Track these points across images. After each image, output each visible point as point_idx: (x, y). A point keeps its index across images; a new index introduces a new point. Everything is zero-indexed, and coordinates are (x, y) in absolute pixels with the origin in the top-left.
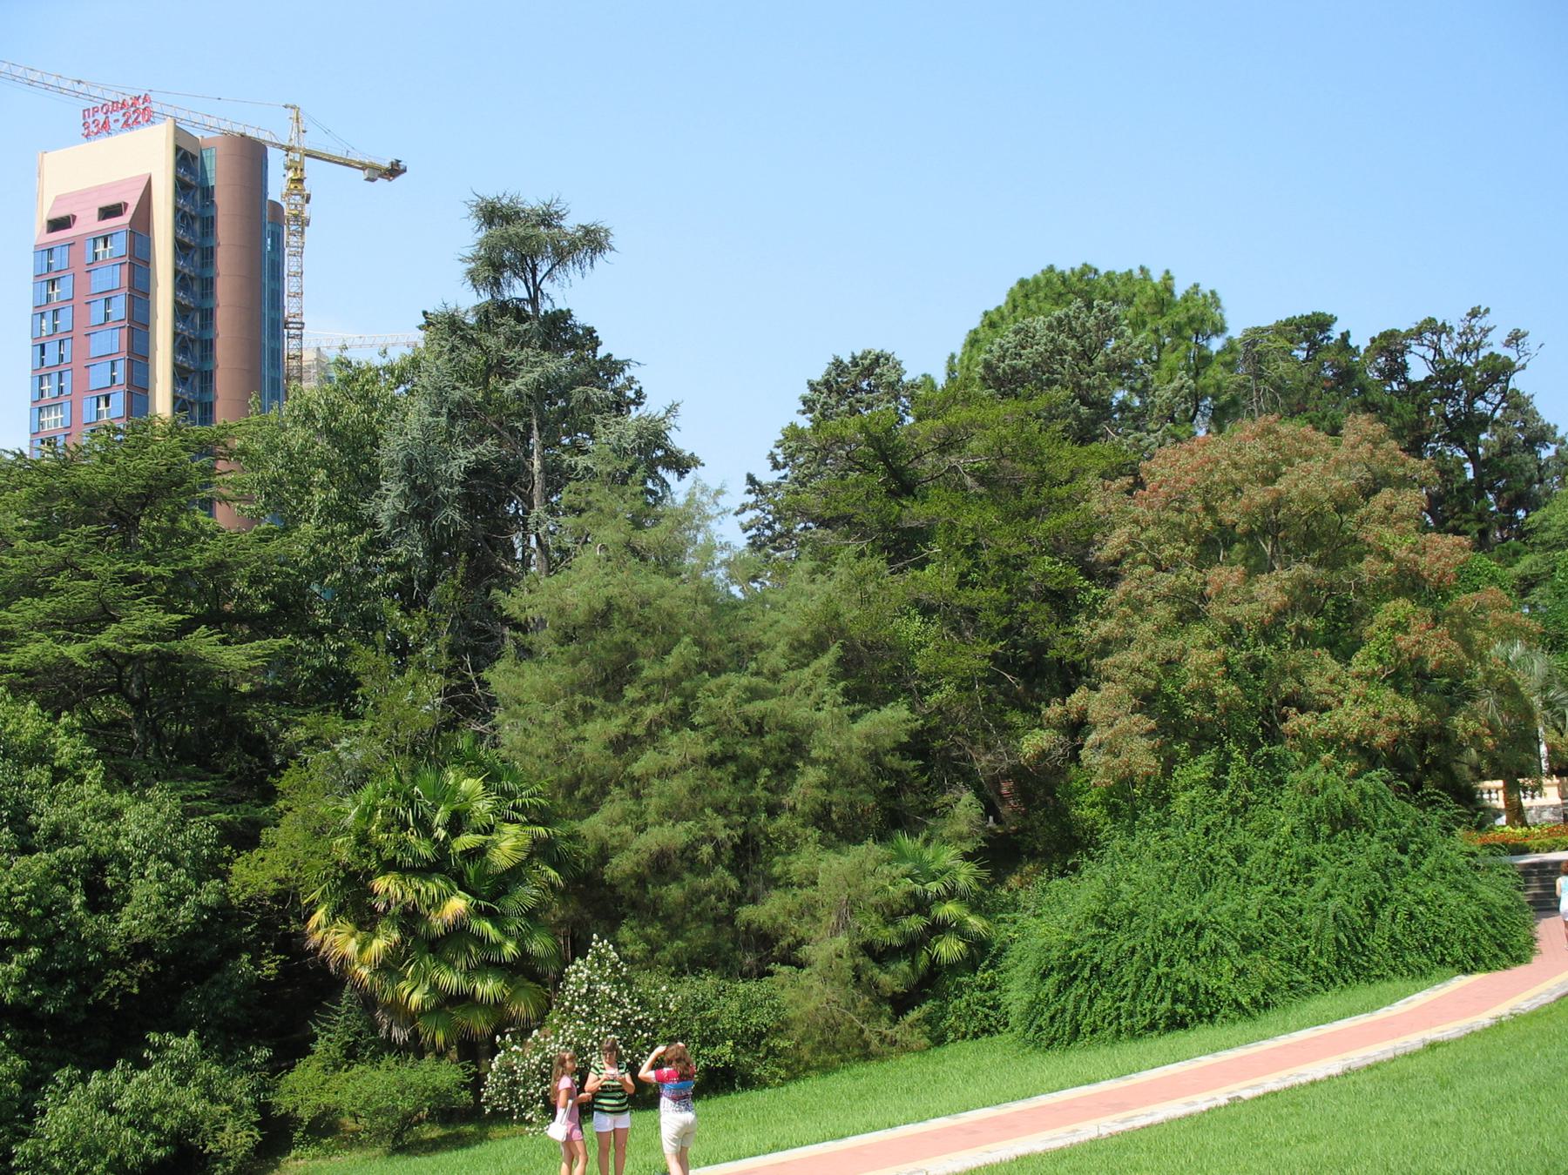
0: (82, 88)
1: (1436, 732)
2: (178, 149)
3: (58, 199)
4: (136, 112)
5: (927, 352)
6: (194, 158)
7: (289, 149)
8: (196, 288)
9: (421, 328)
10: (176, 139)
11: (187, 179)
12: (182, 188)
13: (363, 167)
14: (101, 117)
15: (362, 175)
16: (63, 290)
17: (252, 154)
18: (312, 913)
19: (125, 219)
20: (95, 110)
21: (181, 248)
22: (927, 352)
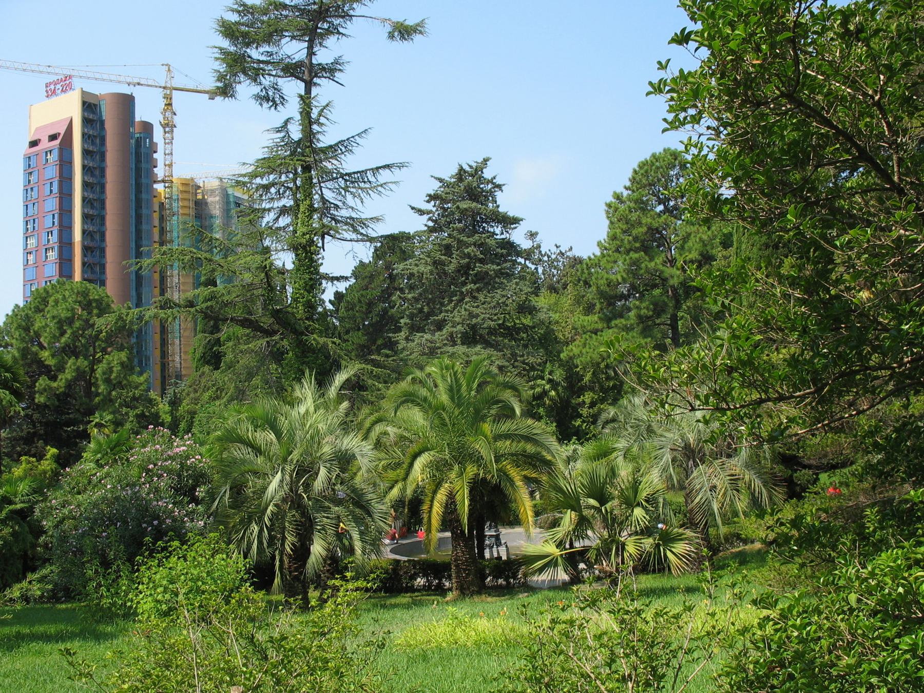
0: (49, 70)
2: (84, 103)
3: (37, 129)
4: (65, 84)
7: (164, 88)
8: (97, 173)
9: (681, 71)
10: (82, 97)
12: (86, 121)
14: (52, 87)
15: (207, 96)
16: (33, 178)
17: (126, 103)
18: (267, 509)
19: (57, 142)
20: (50, 83)
21: (86, 153)
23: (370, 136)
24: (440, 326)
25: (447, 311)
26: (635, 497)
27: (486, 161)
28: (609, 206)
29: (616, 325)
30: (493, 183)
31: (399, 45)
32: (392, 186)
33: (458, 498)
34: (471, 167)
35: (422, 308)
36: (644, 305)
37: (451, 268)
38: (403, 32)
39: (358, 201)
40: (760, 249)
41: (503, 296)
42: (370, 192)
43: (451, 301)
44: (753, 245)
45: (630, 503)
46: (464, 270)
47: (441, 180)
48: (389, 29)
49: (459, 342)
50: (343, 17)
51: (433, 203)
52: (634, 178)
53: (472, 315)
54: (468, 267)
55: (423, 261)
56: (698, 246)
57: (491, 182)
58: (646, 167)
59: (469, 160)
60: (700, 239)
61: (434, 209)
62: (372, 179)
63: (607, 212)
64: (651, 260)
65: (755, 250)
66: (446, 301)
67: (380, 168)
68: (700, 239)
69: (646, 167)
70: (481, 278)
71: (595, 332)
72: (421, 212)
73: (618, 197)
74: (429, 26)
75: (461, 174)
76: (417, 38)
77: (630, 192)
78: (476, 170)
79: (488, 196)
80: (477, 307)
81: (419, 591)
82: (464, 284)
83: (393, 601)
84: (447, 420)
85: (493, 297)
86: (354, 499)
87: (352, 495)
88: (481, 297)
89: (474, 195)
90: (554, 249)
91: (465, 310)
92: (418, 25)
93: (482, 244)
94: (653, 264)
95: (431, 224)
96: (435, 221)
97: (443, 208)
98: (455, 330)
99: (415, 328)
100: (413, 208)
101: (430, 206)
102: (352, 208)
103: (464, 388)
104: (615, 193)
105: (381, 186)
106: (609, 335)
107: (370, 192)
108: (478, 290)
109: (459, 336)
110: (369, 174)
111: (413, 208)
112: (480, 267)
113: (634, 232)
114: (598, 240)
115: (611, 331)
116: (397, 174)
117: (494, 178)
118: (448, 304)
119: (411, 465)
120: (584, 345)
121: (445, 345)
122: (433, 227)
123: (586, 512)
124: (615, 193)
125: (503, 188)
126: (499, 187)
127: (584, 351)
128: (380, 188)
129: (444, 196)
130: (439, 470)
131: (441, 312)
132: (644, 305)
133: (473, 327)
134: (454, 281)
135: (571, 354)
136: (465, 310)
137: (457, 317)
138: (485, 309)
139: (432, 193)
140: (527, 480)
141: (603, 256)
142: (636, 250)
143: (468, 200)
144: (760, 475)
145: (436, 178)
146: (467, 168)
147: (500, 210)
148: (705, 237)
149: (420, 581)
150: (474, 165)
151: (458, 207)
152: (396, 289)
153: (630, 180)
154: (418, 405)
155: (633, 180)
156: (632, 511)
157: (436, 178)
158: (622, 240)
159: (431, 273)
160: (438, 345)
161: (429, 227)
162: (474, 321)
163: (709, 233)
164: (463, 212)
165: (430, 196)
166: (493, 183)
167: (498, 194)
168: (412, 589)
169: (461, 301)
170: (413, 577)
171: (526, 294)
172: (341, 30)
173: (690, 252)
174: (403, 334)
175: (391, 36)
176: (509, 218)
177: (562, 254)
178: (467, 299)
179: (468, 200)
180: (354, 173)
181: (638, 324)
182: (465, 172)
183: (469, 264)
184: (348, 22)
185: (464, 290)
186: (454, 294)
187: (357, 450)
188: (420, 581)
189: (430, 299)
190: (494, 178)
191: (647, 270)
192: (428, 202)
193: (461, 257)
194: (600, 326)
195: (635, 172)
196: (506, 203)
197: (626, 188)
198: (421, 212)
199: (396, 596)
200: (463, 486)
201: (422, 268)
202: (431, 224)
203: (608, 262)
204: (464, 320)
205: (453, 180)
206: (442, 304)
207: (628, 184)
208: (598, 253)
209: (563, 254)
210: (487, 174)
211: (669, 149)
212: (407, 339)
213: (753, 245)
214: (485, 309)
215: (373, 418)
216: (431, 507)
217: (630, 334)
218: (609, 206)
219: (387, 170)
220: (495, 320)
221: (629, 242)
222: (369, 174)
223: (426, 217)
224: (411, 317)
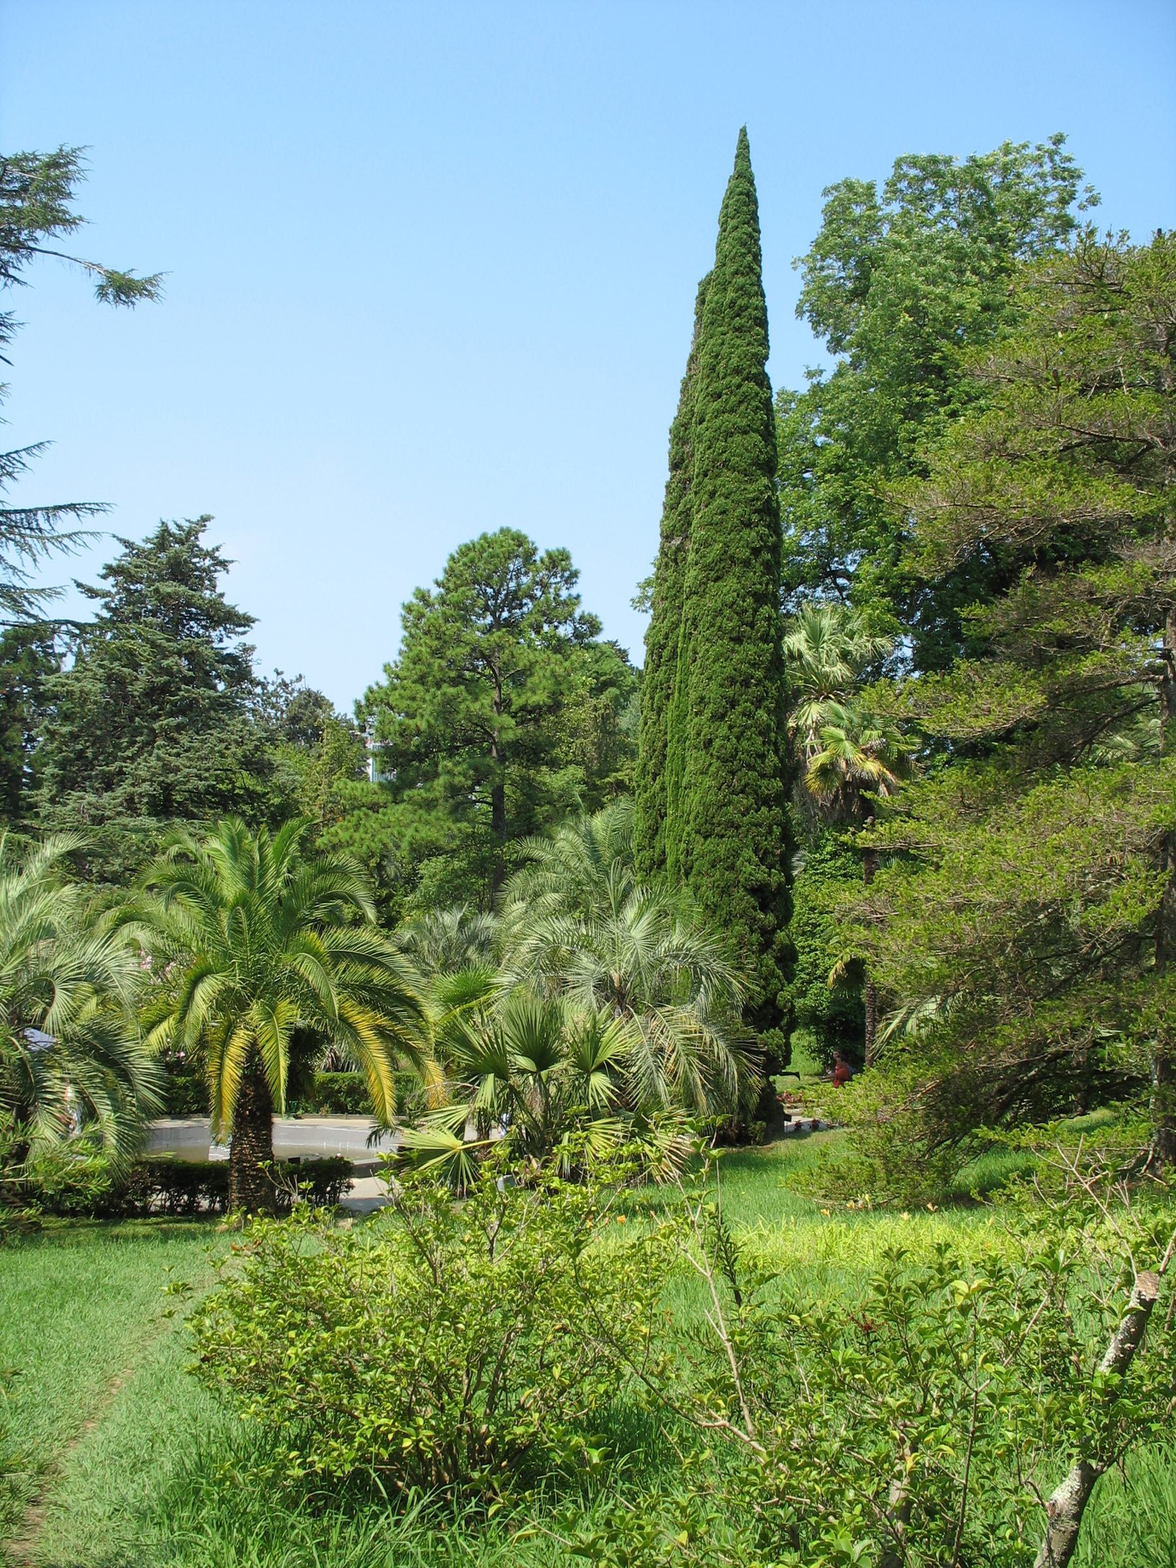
23: (49, 452)
24: (109, 784)
25: (124, 759)
26: (595, 1056)
27: (205, 519)
28: (409, 609)
29: (410, 798)
30: (213, 558)
31: (115, 312)
32: (87, 538)
33: (266, 1054)
34: (180, 527)
35: (82, 751)
36: (459, 769)
37: (137, 689)
38: (121, 288)
39: (27, 557)
40: (721, 686)
41: (221, 741)
42: (48, 545)
43: (132, 743)
44: (710, 679)
45: (585, 1068)
46: (154, 693)
47: (127, 544)
48: (99, 280)
49: (144, 810)
50: (15, 250)
51: (111, 580)
52: (452, 569)
53: (167, 769)
54: (164, 689)
55: (89, 674)
56: (549, 684)
57: (209, 554)
58: (472, 554)
59: (179, 515)
60: (553, 672)
61: (114, 590)
62: (44, 525)
63: (404, 619)
64: (476, 699)
65: (713, 686)
66: (124, 741)
67: (60, 508)
68: (553, 672)
69: (472, 554)
70: (187, 708)
71: (374, 807)
72: (92, 593)
73: (423, 597)
74: (165, 288)
75: (164, 538)
76: (142, 302)
77: (442, 590)
78: (189, 534)
79: (205, 578)
80: (178, 755)
81: (156, 1214)
82: (155, 717)
83: (116, 1230)
84: (245, 925)
85: (203, 741)
86: (98, 1050)
87: (95, 1042)
88: (184, 740)
89: (182, 573)
90: (272, 677)
91: (159, 758)
92: (149, 281)
93: (192, 653)
94: (477, 705)
95: (106, 614)
96: (114, 611)
97: (128, 590)
98: (138, 790)
99: (66, 784)
100: (79, 585)
101: (108, 585)
102: (14, 568)
103: (272, 871)
104: (418, 589)
105: (69, 536)
106: (396, 812)
107: (48, 545)
108: (179, 728)
109: (145, 800)
110: (40, 516)
111: (79, 585)
112: (188, 691)
113: (450, 653)
114: (386, 661)
115: (401, 807)
116: (88, 522)
117: (217, 549)
118: (127, 748)
119: (190, 996)
120: (357, 827)
121: (119, 814)
122: (110, 620)
123: (516, 1080)
124: (418, 589)
125: (230, 567)
126: (223, 564)
127: (357, 836)
128: (66, 541)
129: (133, 570)
130: (231, 1004)
131: (115, 759)
132: (459, 769)
133: (168, 788)
134: (138, 711)
135: (336, 840)
136: (159, 758)
137: (144, 770)
138: (189, 759)
139: (114, 564)
140: (380, 1032)
141: (394, 688)
142: (454, 682)
143: (171, 582)
144: (725, 1034)
145: (120, 540)
146: (173, 529)
147: (226, 601)
148: (560, 671)
149: (158, 1200)
150: (186, 525)
151: (157, 591)
152: (15, 719)
153: (446, 572)
154: (196, 896)
155: (450, 572)
156: (587, 1081)
157: (120, 540)
158: (429, 665)
159: (103, 692)
160: (108, 813)
161: (102, 619)
162: (171, 778)
163: (567, 664)
164: (163, 599)
165: (109, 567)
166: (213, 558)
167: (220, 576)
168: (145, 1213)
169: (150, 743)
170: (146, 1191)
171: (259, 739)
172: (11, 271)
173: (534, 692)
174: (45, 792)
175: (102, 292)
176: (237, 615)
177: (285, 685)
178: (160, 742)
179: (171, 582)
180: (16, 512)
181: (446, 799)
182: (170, 535)
183: (167, 683)
184: (24, 260)
185: (156, 726)
186: (137, 731)
187: (112, 964)
188: (158, 1200)
189: (98, 737)
190: (217, 549)
191: (469, 717)
192: (104, 577)
193: (155, 672)
194: (382, 798)
195: (452, 558)
196: (231, 589)
197: (438, 584)
198: (92, 593)
199: (116, 1224)
200: (274, 1035)
201: (88, 685)
202: (106, 614)
203: (402, 697)
204: (153, 775)
205: (150, 546)
206: (117, 747)
207: (441, 577)
208: (384, 681)
209: (286, 685)
210: (205, 541)
211: (508, 530)
212: (52, 801)
213: (710, 679)
214: (189, 759)
215: (114, 913)
216: (221, 1067)
217: (434, 813)
218: (409, 609)
219: (72, 514)
220: (206, 779)
221: (441, 668)
222: (40, 516)
223: (99, 602)
224: (62, 765)
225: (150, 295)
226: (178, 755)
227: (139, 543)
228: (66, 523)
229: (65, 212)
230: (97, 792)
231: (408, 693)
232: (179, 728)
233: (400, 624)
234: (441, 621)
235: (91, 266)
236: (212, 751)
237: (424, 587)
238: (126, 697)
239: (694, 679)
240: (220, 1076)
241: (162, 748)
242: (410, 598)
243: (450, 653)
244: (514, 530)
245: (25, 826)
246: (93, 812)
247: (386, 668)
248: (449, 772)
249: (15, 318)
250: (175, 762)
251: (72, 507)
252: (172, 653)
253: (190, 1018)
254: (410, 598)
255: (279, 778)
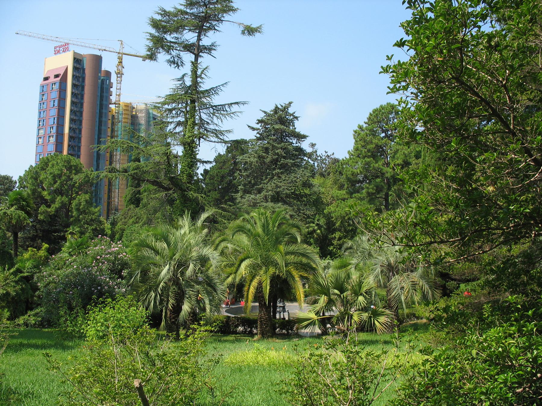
0: (57, 39)
1: (83, 309)
2: (75, 59)
3: (48, 71)
4: (65, 48)
5: (22, 175)
6: (81, 60)
7: (119, 53)
8: (79, 97)
11: (78, 66)
12: (75, 69)
13: (140, 57)
14: (58, 49)
15: (141, 59)
17: (98, 60)
20: (57, 47)
21: (74, 86)
22: (22, 175)
24: (260, 191)
25: (264, 183)
27: (290, 103)
28: (355, 132)
29: (355, 197)
31: (247, 38)
33: (264, 285)
34: (282, 106)
37: (268, 160)
38: (250, 31)
40: (436, 161)
41: (295, 177)
44: (432, 158)
45: (357, 293)
46: (275, 162)
47: (265, 112)
48: (242, 28)
49: (270, 200)
50: (218, 21)
51: (260, 124)
52: (370, 118)
53: (277, 187)
56: (402, 157)
59: (281, 102)
60: (404, 153)
61: (261, 128)
62: (228, 109)
63: (354, 135)
64: (376, 162)
67: (233, 103)
68: (404, 153)
71: (344, 200)
72: (253, 129)
73: (361, 127)
74: (264, 29)
76: (257, 34)
77: (367, 125)
80: (281, 182)
82: (274, 169)
85: (289, 178)
89: (283, 122)
90: (324, 154)
91: (274, 183)
92: (258, 28)
93: (285, 148)
94: (377, 165)
98: (268, 194)
99: (246, 192)
100: (249, 127)
102: (216, 124)
104: (359, 125)
105: (233, 113)
106: (351, 202)
108: (282, 173)
111: (249, 127)
113: (368, 147)
115: (352, 199)
116: (242, 108)
119: (239, 265)
122: (260, 137)
123: (332, 297)
124: (359, 125)
125: (299, 119)
126: (297, 118)
127: (337, 210)
128: (232, 115)
130: (254, 269)
131: (261, 184)
132: (371, 186)
133: (278, 193)
135: (330, 211)
136: (274, 183)
140: (302, 277)
143: (279, 124)
144: (428, 282)
145: (263, 111)
146: (280, 107)
147: (296, 130)
148: (406, 152)
149: (240, 329)
150: (284, 105)
151: (273, 128)
152: (237, 170)
154: (245, 233)
155: (369, 119)
157: (263, 111)
158: (361, 151)
163: (409, 150)
164: (276, 130)
165: (259, 120)
166: (293, 116)
167: (296, 122)
168: (236, 333)
170: (237, 326)
171: (308, 177)
172: (216, 28)
174: (239, 194)
175: (243, 33)
176: (301, 135)
177: (328, 156)
178: (275, 178)
179: (279, 124)
181: (367, 197)
182: (279, 109)
183: (277, 158)
185: (274, 172)
187: (210, 255)
188: (240, 329)
192: (258, 123)
194: (346, 197)
195: (371, 114)
196: (299, 127)
197: (365, 123)
198: (253, 129)
199: (227, 336)
203: (353, 162)
205: (272, 113)
206: (262, 180)
207: (367, 121)
208: (348, 157)
209: (329, 156)
210: (291, 111)
211: (390, 103)
212: (241, 197)
213: (432, 158)
216: (249, 289)
218: (355, 132)
220: (290, 190)
221: (365, 152)
223: (256, 132)
224: (245, 185)
225: (259, 32)
226: (281, 182)
227: (269, 112)
228: (235, 108)
229: (233, 7)
230: (256, 195)
231: (355, 161)
232: (282, 173)
233: (353, 137)
234: (126, 174)
235: (240, 24)
236: (292, 181)
237: (361, 124)
238: (264, 163)
239: (427, 158)
240: (248, 291)
241: (276, 180)
242: (356, 128)
243: (368, 147)
244: (392, 103)
245: (222, 207)
246: (253, 201)
247: (349, 152)
248: (367, 188)
249: (217, 43)
250: (280, 184)
251: (237, 103)
252: (279, 148)
253: (239, 272)
254: (356, 128)
255: (315, 189)
